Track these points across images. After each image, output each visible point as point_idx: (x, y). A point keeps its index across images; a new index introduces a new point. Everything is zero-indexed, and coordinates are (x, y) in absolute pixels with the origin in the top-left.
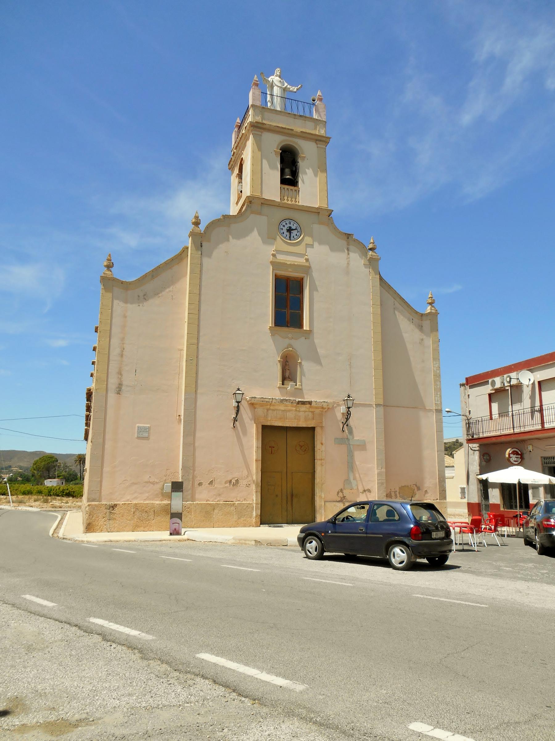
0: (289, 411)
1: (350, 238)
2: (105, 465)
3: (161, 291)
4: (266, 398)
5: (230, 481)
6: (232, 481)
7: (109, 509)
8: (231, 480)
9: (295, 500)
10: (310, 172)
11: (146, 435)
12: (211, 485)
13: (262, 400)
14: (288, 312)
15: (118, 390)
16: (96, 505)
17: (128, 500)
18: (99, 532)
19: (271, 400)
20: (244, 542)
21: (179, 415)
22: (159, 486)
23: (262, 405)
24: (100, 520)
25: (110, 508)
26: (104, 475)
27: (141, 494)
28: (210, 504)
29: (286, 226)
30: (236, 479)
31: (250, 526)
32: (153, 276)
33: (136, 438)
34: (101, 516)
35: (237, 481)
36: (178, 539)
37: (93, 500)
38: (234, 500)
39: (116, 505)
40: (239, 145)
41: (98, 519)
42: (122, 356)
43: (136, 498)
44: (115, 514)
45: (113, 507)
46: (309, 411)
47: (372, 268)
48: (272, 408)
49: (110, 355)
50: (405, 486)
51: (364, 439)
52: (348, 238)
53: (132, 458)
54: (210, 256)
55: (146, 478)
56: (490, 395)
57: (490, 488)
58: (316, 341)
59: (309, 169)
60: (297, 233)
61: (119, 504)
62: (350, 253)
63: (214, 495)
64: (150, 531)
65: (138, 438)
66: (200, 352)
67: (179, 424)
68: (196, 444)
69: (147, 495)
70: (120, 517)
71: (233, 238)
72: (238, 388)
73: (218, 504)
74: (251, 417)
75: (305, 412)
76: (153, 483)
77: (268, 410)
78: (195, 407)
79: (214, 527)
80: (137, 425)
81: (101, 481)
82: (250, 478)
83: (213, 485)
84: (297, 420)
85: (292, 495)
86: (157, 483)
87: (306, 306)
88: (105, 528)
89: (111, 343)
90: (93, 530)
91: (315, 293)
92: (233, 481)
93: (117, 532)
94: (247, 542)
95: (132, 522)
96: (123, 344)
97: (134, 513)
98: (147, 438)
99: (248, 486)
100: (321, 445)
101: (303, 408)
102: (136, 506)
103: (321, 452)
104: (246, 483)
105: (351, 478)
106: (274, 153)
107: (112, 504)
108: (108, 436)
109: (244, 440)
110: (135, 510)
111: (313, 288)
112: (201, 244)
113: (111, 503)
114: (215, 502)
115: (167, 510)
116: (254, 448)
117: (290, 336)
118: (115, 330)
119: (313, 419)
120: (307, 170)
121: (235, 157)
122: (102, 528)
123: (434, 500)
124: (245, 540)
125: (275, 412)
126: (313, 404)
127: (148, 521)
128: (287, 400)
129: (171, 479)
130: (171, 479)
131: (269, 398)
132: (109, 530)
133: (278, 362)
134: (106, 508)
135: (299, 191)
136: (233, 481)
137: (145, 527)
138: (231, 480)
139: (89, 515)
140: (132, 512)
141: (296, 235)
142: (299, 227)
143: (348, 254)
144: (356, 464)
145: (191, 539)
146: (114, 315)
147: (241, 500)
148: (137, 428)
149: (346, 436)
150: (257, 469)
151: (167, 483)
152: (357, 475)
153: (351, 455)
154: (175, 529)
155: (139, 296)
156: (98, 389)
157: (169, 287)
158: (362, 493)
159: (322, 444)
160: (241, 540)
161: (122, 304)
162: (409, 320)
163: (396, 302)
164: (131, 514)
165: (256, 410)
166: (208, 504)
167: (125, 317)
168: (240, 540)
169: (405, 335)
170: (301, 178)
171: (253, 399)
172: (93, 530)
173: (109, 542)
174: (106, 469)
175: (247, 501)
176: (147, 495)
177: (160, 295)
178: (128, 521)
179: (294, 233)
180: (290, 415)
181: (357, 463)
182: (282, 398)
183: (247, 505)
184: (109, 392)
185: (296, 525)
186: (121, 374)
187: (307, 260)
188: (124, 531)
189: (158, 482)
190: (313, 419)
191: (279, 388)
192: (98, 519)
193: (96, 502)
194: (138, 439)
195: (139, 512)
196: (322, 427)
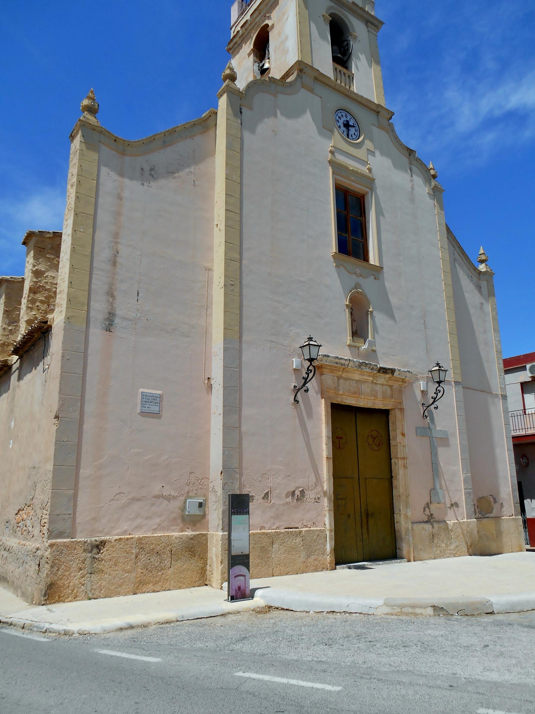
0: (365, 382)
1: (411, 155)
2: (83, 464)
3: (178, 171)
4: (341, 359)
5: (293, 493)
6: (296, 492)
7: (91, 552)
8: (294, 492)
9: (371, 522)
10: (362, 57)
11: (155, 409)
12: (266, 501)
13: (337, 360)
14: (350, 238)
15: (107, 323)
16: (65, 545)
17: (125, 533)
18: (70, 601)
19: (347, 363)
20: (410, 610)
21: (209, 378)
22: (176, 504)
23: (333, 370)
24: (72, 575)
25: (92, 550)
26: (82, 483)
27: (147, 518)
28: (267, 534)
29: (342, 118)
30: (301, 489)
31: (323, 568)
32: (164, 142)
33: (139, 414)
34: (74, 566)
35: (302, 492)
36: (252, 609)
37: (60, 535)
38: (299, 525)
39: (103, 543)
40: (260, 8)
41: (69, 574)
42: (114, 264)
43: (138, 528)
44: (102, 560)
45: (97, 547)
46: (387, 385)
47: (437, 201)
48: (344, 375)
49: (94, 260)
50: (483, 497)
51: (446, 430)
52: (410, 155)
53: (132, 451)
54: (253, 131)
55: (156, 489)
56: (522, 384)
57: (526, 499)
58: (387, 284)
59: (362, 55)
60: (355, 132)
61: (109, 541)
62: (414, 175)
63: (272, 517)
64: (165, 590)
65: (143, 413)
66: (244, 275)
67: (208, 393)
68: (243, 429)
69: (158, 520)
70: (110, 567)
71: (282, 114)
72: (309, 337)
73: (278, 534)
74: (317, 388)
75: (382, 385)
76: (169, 498)
77: (339, 378)
78: (240, 366)
79: (273, 576)
80: (141, 390)
81: (75, 497)
82: (319, 488)
83: (270, 500)
84: (374, 396)
85: (367, 515)
86: (175, 498)
87: (372, 231)
88: (83, 591)
89: (96, 238)
90: (59, 597)
91: (381, 217)
92: (297, 493)
93: (105, 597)
94: (418, 611)
95: (134, 574)
96: (117, 243)
97: (136, 557)
98: (157, 415)
99: (317, 500)
100: (401, 436)
101: (382, 379)
102: (140, 543)
103: (402, 447)
104: (313, 496)
105: (438, 487)
106: (322, 18)
107: (96, 541)
108: (89, 408)
109: (309, 425)
110: (138, 551)
111: (379, 213)
112: (241, 109)
113: (93, 539)
114: (273, 531)
115: (192, 548)
116: (324, 439)
117: (358, 271)
118: (103, 217)
119: (392, 397)
120: (360, 55)
121: (246, 29)
122: (77, 592)
123: (510, 516)
124: (413, 607)
125: (348, 382)
126: (396, 374)
127: (161, 571)
128: (367, 364)
129: (197, 490)
130: (197, 490)
131: (346, 358)
132: (90, 595)
133: (345, 307)
134: (85, 551)
135: (353, 78)
136: (297, 493)
137: (156, 583)
138: (294, 492)
139: (52, 567)
140: (134, 556)
141: (354, 134)
142: (357, 125)
143: (412, 176)
144: (440, 465)
145: (276, 605)
146: (101, 192)
147: (309, 526)
148: (140, 396)
149: (427, 424)
150: (328, 472)
151: (191, 497)
152: (443, 482)
153: (434, 454)
154: (239, 588)
155: (142, 169)
156: (72, 317)
157: (189, 166)
158: (450, 508)
159: (403, 435)
160: (405, 606)
161: (114, 176)
162: (468, 276)
163: (455, 251)
164: (131, 560)
165: (323, 377)
166: (264, 533)
167: (120, 198)
168: (401, 606)
169: (467, 295)
170: (354, 61)
171: (325, 358)
172: (59, 597)
173: (126, 629)
174: (85, 471)
175: (317, 526)
176: (158, 520)
177: (176, 175)
178: (127, 574)
179: (352, 131)
180: (366, 388)
181: (442, 464)
182: (361, 361)
183: (317, 533)
184: (92, 325)
185: (381, 563)
186: (113, 296)
187: (370, 170)
188: (118, 594)
189: (177, 496)
190: (392, 397)
191: (349, 346)
192: (69, 574)
193: (65, 538)
194: (142, 416)
195: (145, 554)
196: (402, 410)
